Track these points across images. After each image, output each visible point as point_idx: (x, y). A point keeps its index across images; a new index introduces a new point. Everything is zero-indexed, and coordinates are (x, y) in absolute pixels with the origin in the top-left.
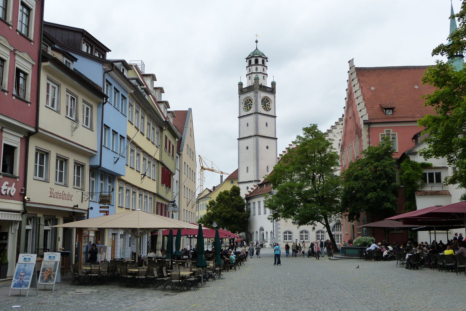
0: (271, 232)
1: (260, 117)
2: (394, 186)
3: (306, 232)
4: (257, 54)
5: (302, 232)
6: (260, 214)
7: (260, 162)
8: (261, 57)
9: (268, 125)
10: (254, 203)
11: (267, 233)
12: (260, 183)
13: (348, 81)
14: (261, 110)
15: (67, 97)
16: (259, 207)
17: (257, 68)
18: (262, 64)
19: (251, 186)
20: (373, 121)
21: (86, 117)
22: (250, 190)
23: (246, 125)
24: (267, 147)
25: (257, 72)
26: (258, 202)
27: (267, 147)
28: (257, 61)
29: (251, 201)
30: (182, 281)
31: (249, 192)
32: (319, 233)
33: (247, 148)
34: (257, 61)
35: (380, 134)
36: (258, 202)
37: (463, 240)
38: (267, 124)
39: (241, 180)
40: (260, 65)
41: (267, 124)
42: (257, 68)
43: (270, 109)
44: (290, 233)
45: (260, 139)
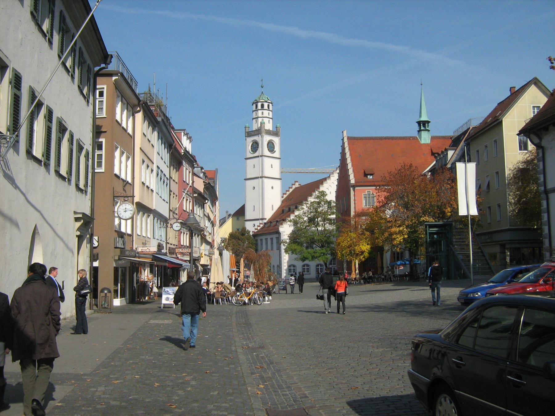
0: (278, 266)
1: (266, 159)
2: (353, 216)
3: (308, 265)
4: (262, 99)
5: (318, 265)
6: (272, 249)
7: (266, 201)
8: (266, 102)
9: (273, 166)
10: (261, 240)
11: (274, 266)
12: (265, 221)
13: (341, 153)
14: (267, 152)
15: (282, 212)
16: (272, 243)
17: (263, 112)
18: (267, 109)
19: (258, 223)
20: (358, 184)
21: (51, 122)
22: (256, 227)
23: (253, 166)
24: (272, 187)
25: (264, 116)
26: (271, 238)
27: (272, 187)
28: (262, 106)
29: (259, 238)
30: (507, 249)
31: (256, 229)
32: (319, 266)
33: (254, 188)
34: (262, 106)
35: (363, 194)
36: (271, 238)
37: (60, 302)
38: (272, 165)
39: (248, 216)
40: (266, 110)
41: (272, 165)
42: (263, 112)
43: (275, 151)
44: (294, 266)
45: (265, 180)
